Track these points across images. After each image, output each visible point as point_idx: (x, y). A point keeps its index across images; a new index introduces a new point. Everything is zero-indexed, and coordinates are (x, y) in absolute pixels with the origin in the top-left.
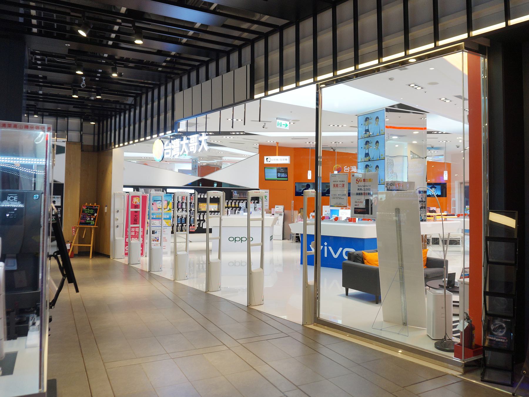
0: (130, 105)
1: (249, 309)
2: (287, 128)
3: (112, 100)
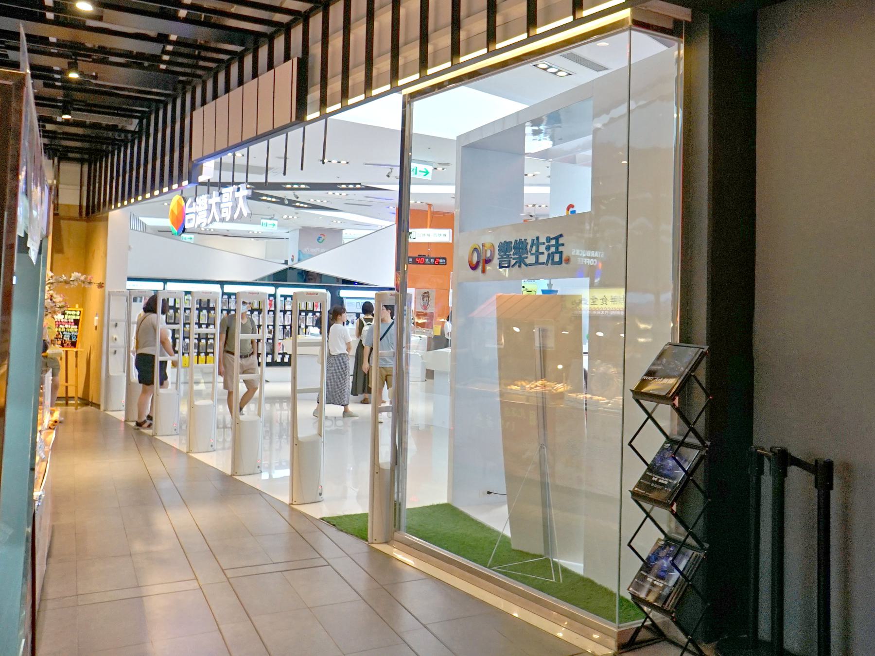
0: (133, 133)
2: (429, 177)
3: (104, 123)
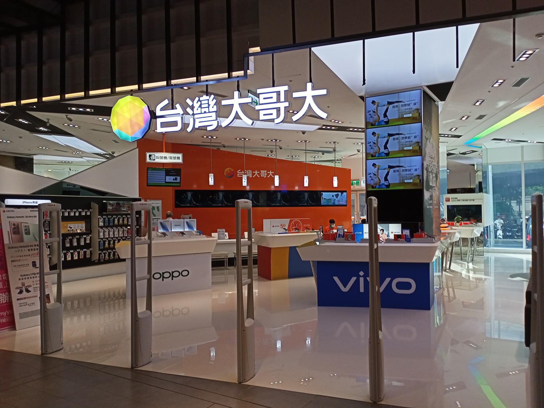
1: (242, 388)
